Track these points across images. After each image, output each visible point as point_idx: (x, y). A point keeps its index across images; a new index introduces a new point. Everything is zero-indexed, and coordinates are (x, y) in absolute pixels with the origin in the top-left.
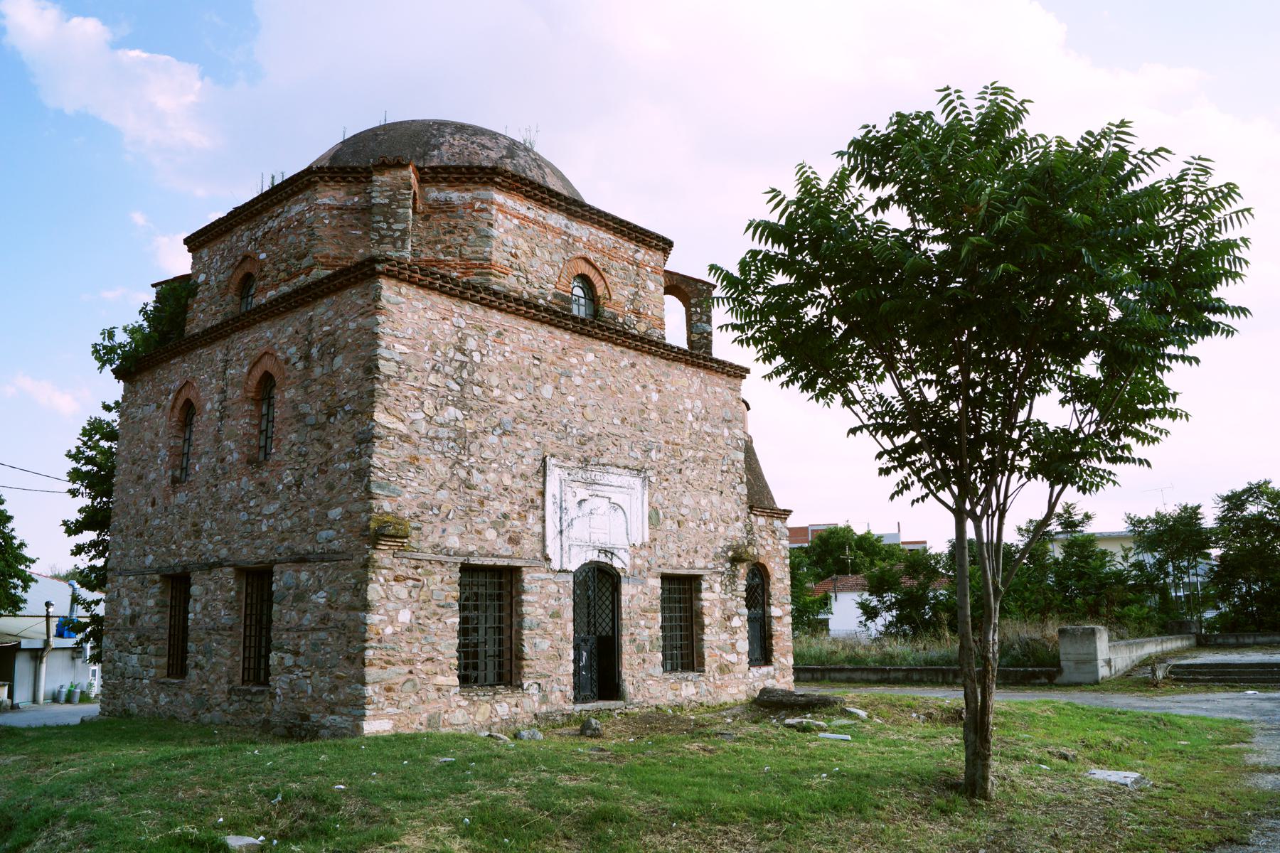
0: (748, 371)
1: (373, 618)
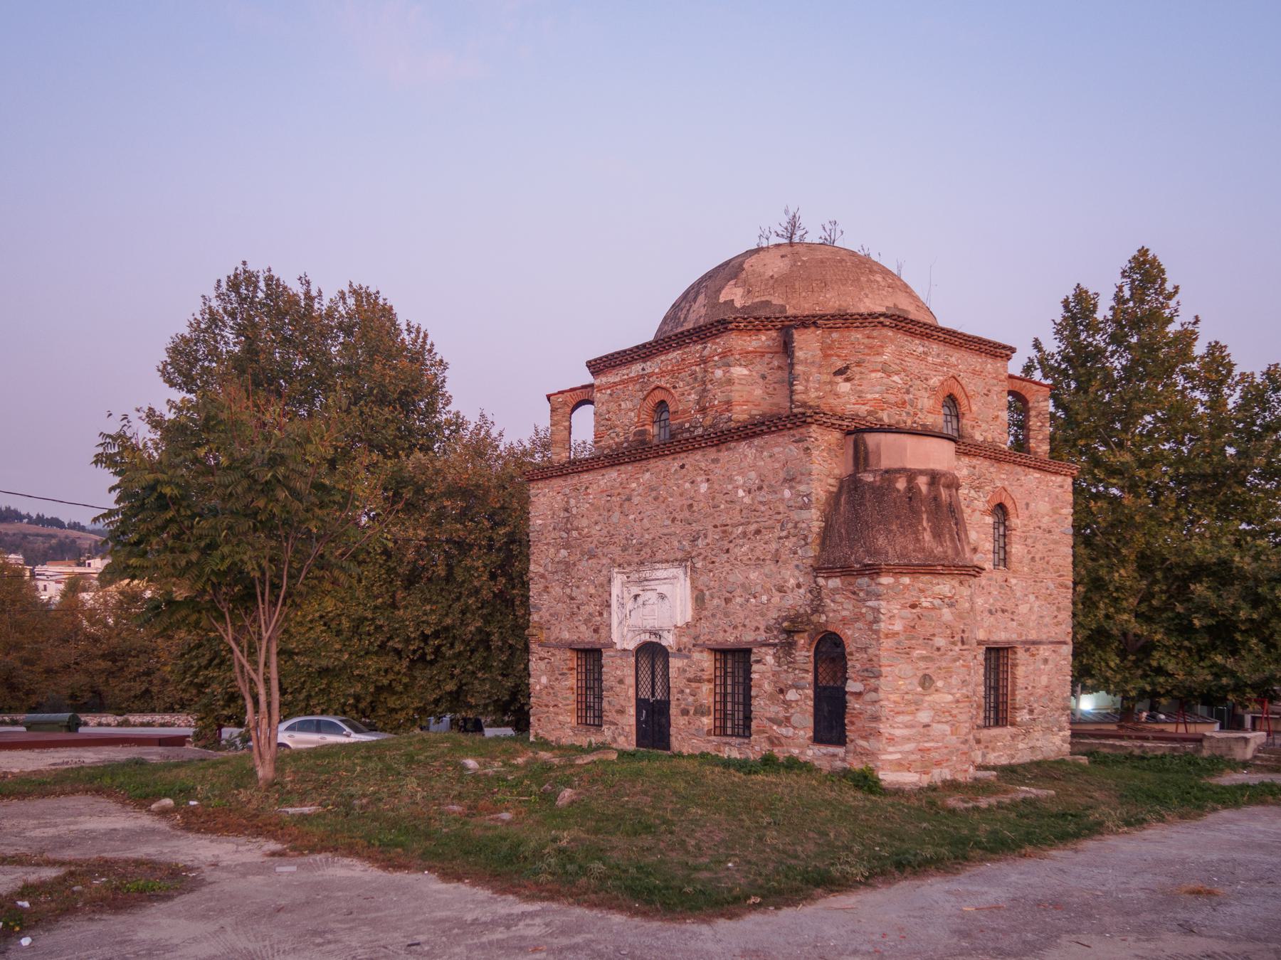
0: (1013, 350)
1: (532, 680)
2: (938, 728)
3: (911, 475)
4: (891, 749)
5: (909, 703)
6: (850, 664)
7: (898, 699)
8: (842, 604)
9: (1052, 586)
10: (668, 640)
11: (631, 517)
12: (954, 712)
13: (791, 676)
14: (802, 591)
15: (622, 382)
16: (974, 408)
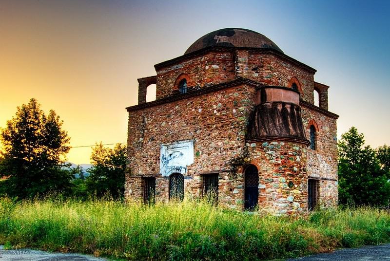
2: (296, 204)
3: (284, 104)
6: (260, 177)
7: (280, 191)
8: (257, 153)
9: (331, 159)
10: (183, 172)
11: (170, 123)
12: (301, 198)
13: (235, 183)
14: (240, 149)
15: (168, 72)
16: (303, 89)
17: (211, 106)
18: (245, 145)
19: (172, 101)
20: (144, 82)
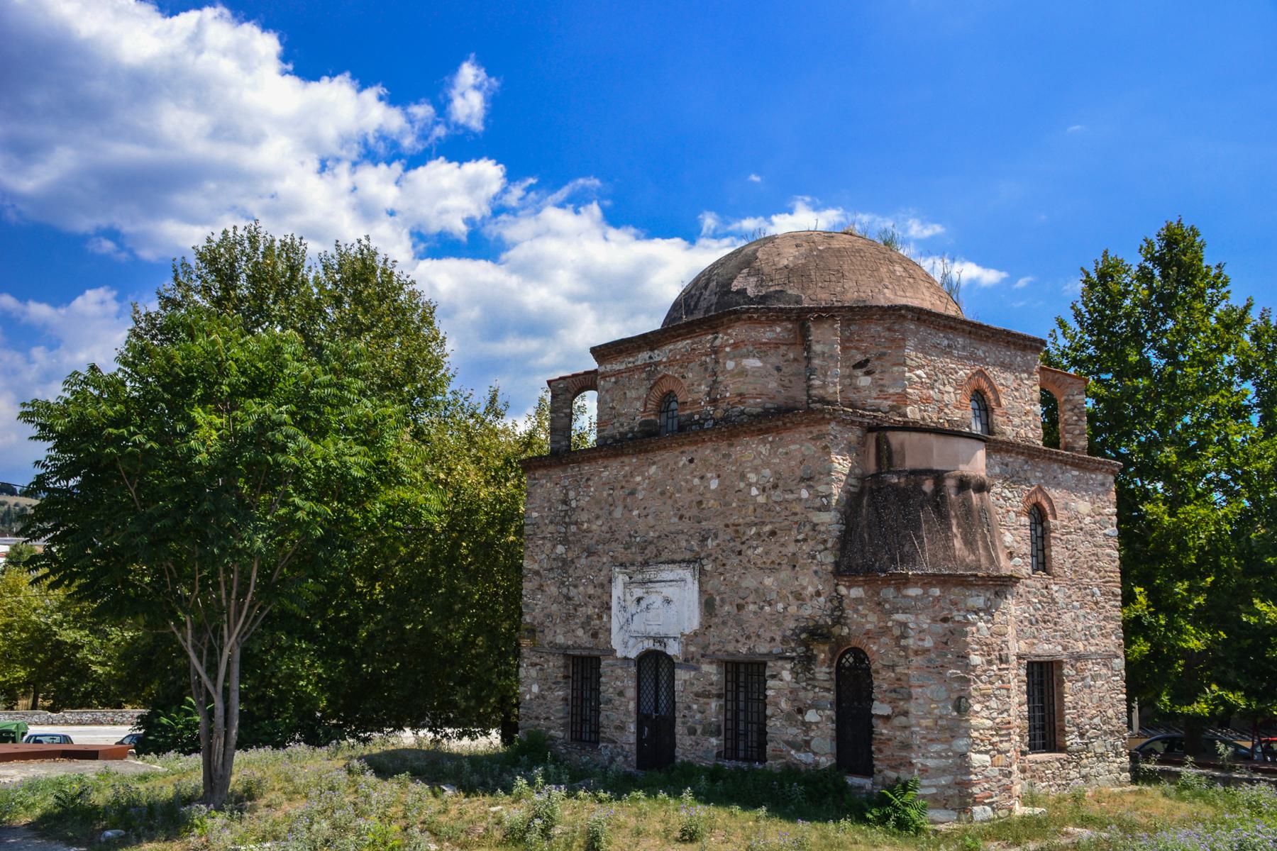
4: (925, 782)
5: (943, 729)
6: (876, 683)
10: (673, 649)
11: (635, 513)
14: (822, 599)
16: (1003, 402)
17: (743, 477)
18: (836, 591)
19: (640, 452)
20: (566, 389)
